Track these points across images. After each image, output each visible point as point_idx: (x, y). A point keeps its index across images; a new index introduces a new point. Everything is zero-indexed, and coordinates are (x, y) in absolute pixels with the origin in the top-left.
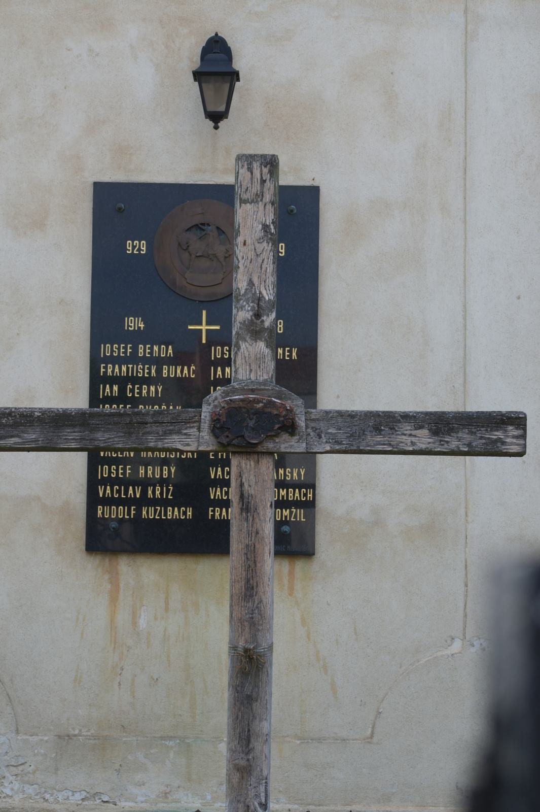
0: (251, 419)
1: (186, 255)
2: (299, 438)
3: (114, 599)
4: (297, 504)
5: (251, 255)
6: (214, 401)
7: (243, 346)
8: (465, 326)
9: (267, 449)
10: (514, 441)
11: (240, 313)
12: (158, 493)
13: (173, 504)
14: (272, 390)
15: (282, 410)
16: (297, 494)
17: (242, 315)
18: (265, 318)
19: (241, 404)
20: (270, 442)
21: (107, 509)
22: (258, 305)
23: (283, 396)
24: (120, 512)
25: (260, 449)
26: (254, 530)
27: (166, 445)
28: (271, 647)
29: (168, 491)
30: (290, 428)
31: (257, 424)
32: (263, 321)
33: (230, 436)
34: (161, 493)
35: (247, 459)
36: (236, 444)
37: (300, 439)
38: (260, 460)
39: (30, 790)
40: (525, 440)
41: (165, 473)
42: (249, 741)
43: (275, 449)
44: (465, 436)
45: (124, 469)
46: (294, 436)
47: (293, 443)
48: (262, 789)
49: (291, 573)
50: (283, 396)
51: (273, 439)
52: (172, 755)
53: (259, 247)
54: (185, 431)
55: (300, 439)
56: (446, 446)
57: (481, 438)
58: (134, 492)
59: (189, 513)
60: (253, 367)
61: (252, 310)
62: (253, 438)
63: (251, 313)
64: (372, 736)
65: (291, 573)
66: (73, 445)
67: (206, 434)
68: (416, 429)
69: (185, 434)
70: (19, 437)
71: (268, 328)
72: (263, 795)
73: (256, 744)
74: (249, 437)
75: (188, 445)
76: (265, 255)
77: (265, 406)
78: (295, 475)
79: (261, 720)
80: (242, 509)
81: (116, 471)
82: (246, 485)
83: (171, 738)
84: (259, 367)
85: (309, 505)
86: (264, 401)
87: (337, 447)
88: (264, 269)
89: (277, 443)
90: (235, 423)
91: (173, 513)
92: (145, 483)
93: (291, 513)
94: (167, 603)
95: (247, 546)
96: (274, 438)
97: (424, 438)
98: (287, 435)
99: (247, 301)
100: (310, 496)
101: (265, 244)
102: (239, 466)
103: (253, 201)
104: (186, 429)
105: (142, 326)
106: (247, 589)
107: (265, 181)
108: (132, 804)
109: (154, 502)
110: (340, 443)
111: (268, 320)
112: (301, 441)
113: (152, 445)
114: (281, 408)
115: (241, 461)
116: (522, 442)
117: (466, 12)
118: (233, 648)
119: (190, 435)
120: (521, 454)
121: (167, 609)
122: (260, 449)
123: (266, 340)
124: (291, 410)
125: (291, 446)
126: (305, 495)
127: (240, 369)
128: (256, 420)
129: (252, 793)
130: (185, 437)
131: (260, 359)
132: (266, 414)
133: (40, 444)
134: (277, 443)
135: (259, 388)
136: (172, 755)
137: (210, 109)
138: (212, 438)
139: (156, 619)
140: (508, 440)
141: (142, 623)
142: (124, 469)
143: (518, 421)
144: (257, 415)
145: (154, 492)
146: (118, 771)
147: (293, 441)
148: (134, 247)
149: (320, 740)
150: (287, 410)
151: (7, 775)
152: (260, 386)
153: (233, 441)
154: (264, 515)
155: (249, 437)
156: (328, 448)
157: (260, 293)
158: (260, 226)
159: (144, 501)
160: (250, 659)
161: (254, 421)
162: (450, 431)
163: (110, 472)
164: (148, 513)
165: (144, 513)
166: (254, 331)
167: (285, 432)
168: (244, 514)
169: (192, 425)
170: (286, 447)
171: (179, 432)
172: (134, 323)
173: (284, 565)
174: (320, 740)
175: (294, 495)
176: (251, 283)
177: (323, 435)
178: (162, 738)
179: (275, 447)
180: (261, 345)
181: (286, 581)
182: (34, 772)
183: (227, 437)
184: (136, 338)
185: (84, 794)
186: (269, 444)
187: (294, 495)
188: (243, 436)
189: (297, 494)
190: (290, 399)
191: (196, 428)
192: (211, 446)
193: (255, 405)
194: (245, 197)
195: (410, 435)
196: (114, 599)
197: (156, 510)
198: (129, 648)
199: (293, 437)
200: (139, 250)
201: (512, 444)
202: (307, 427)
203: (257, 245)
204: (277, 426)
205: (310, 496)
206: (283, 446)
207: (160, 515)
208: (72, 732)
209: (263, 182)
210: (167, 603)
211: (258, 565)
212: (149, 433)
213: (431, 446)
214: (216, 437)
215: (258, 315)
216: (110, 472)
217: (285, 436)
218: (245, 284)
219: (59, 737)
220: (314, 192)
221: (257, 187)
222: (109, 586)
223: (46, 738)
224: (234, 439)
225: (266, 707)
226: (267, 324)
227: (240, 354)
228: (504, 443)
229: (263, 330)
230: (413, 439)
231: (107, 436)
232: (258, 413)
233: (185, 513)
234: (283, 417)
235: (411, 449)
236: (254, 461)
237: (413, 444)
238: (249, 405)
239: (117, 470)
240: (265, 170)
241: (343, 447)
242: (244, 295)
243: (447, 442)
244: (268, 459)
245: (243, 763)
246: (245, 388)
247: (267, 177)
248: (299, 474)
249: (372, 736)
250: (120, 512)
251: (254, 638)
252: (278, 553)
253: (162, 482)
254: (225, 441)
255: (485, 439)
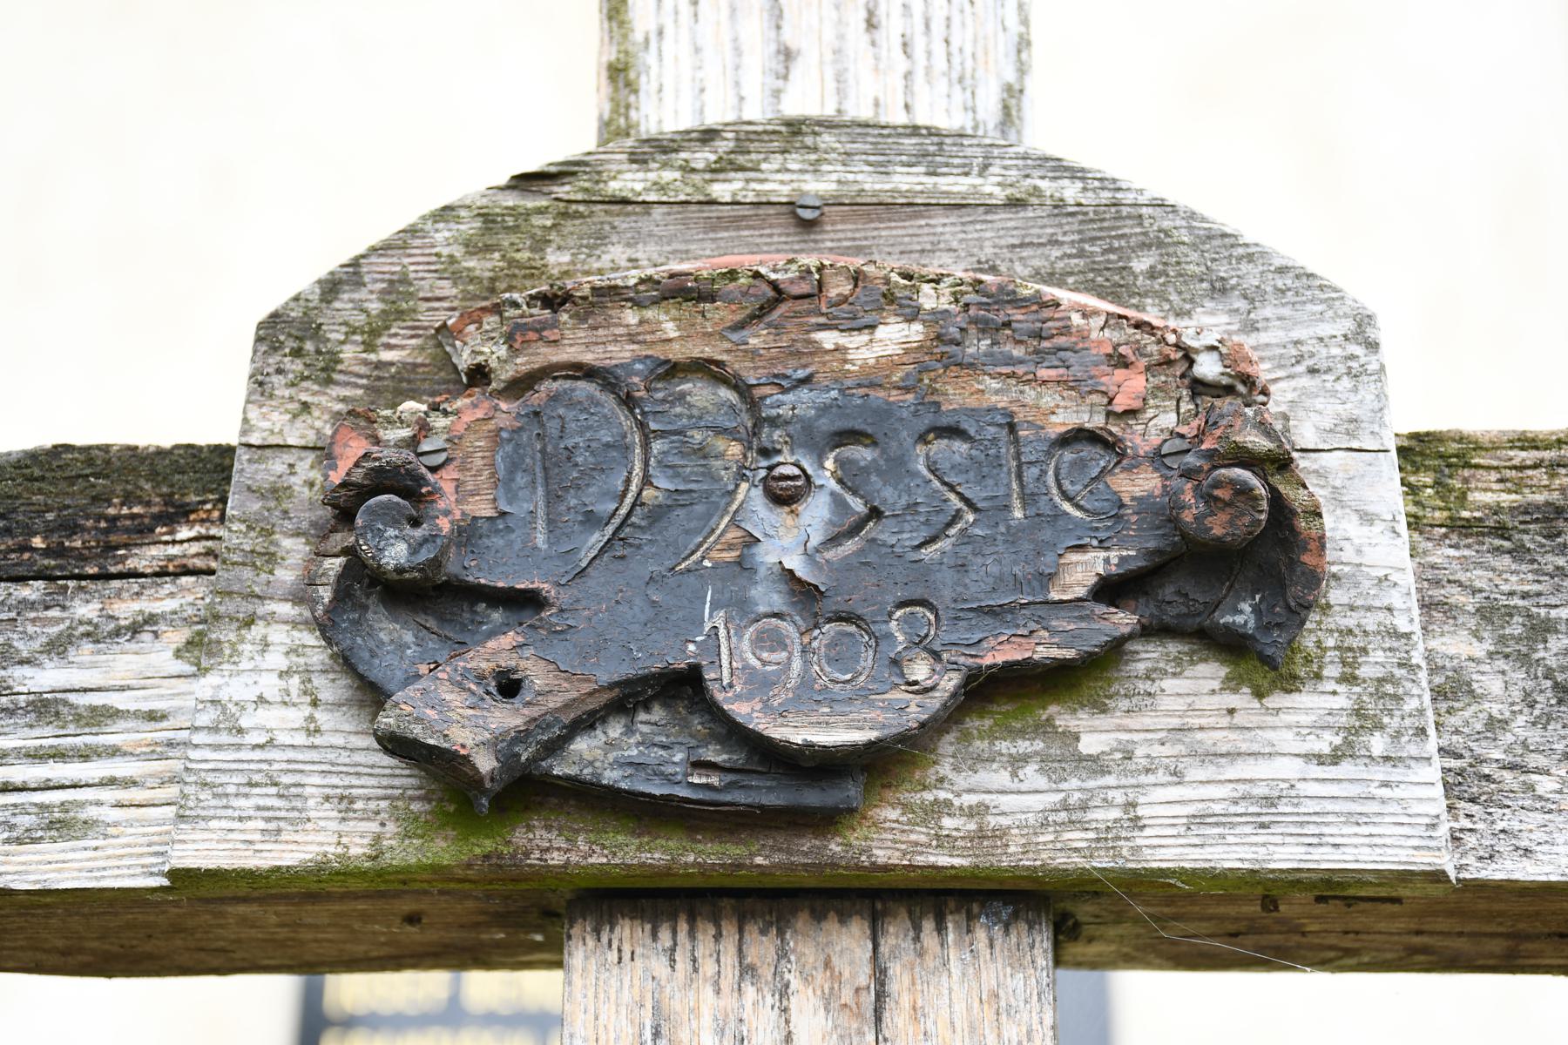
0: (784, 496)
2: (1358, 712)
6: (372, 336)
9: (981, 834)
14: (1015, 204)
15: (1131, 386)
19: (670, 329)
20: (1016, 763)
23: (1141, 264)
31: (850, 546)
33: (537, 676)
35: (747, 971)
36: (611, 776)
37: (1364, 720)
38: (899, 979)
43: (1076, 837)
46: (1290, 683)
47: (1288, 768)
50: (1141, 264)
51: (1045, 729)
54: (47, 677)
55: (1364, 720)
62: (810, 696)
67: (270, 685)
69: (45, 708)
74: (760, 684)
84: (871, 24)
86: (928, 299)
89: (1096, 766)
90: (596, 539)
96: (1065, 718)
98: (1209, 673)
104: (58, 647)
112: (1378, 744)
114: (1123, 363)
115: (677, 1003)
119: (101, 716)
127: (676, 47)
128: (838, 503)
130: (44, 736)
132: (954, 432)
134: (1096, 766)
135: (870, 183)
144: (862, 454)
147: (1286, 740)
150: (1199, 387)
152: (882, 169)
153: (582, 745)
155: (760, 684)
161: (816, 514)
167: (1173, 648)
169: (126, 609)
170: (1199, 819)
179: (1073, 813)
183: (509, 686)
186: (1000, 777)
190: (1220, 289)
191: (179, 637)
192: (325, 816)
193: (828, 339)
199: (1276, 700)
224: (587, 723)
234: (1158, 458)
236: (828, 1000)
238: (757, 339)
244: (989, 978)
246: (721, 190)
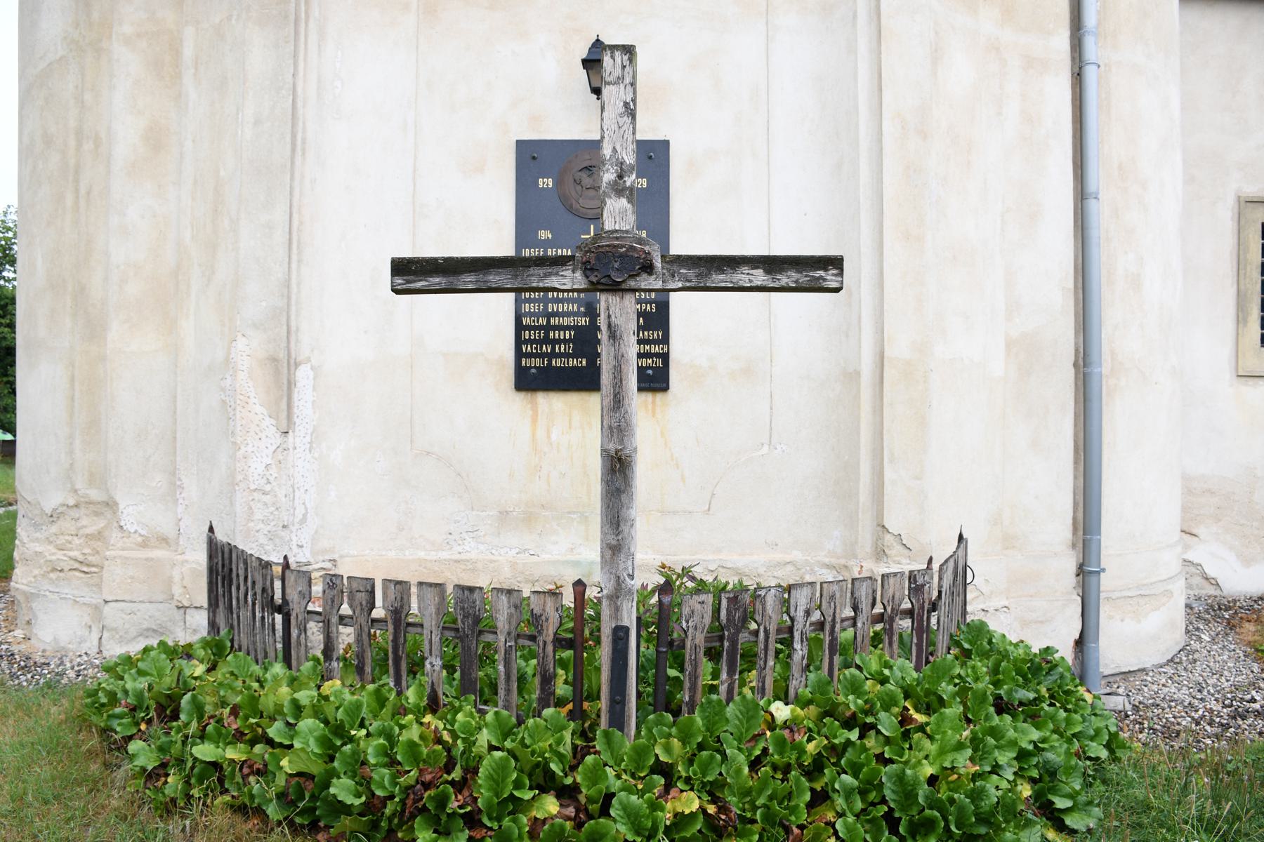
1: (579, 188)
3: (534, 420)
4: (657, 355)
5: (614, 127)
7: (608, 201)
8: (769, 234)
10: (834, 278)
11: (606, 175)
12: (562, 349)
13: (573, 356)
16: (657, 349)
17: (608, 176)
18: (626, 179)
21: (528, 360)
22: (621, 168)
24: (538, 362)
25: (623, 286)
26: (620, 354)
27: (546, 285)
28: (635, 450)
29: (569, 347)
30: (648, 268)
32: (625, 181)
34: (565, 349)
39: (482, 547)
40: (842, 277)
41: (567, 335)
42: (618, 525)
44: (794, 275)
45: (540, 333)
48: (630, 563)
49: (654, 402)
52: (575, 524)
53: (621, 121)
56: (777, 282)
57: (806, 276)
58: (547, 349)
59: (584, 362)
60: (618, 219)
61: (616, 172)
62: (618, 277)
63: (615, 175)
64: (709, 510)
65: (654, 402)
66: (470, 286)
68: (752, 269)
69: (562, 276)
70: (426, 281)
71: (629, 187)
72: (630, 568)
73: (624, 527)
75: (564, 284)
76: (625, 127)
77: (627, 250)
78: (655, 335)
79: (628, 508)
80: (610, 337)
81: (534, 335)
82: (613, 317)
83: (574, 513)
85: (665, 357)
87: (688, 284)
88: (625, 138)
91: (573, 362)
92: (555, 342)
93: (653, 361)
94: (570, 423)
95: (615, 366)
97: (759, 277)
99: (612, 165)
100: (666, 349)
101: (626, 118)
102: (607, 301)
103: (615, 83)
105: (550, 236)
106: (615, 402)
107: (625, 67)
108: (550, 556)
109: (560, 355)
110: (690, 281)
111: (630, 180)
113: (534, 285)
116: (840, 279)
117: (767, 23)
118: (604, 451)
120: (837, 290)
121: (570, 428)
122: (623, 286)
123: (627, 197)
124: (649, 253)
125: (650, 284)
126: (662, 349)
129: (622, 566)
131: (623, 213)
133: (443, 286)
136: (575, 524)
137: (593, 86)
138: (584, 278)
139: (563, 433)
140: (828, 278)
141: (554, 437)
142: (540, 333)
143: (836, 263)
145: (560, 349)
146: (540, 534)
148: (544, 183)
149: (675, 513)
151: (466, 537)
154: (628, 341)
156: (680, 285)
157: (623, 158)
158: (622, 104)
159: (553, 355)
160: (620, 459)
162: (781, 271)
163: (530, 336)
164: (556, 363)
165: (554, 362)
166: (619, 189)
168: (612, 341)
171: (557, 274)
172: (545, 235)
173: (648, 397)
174: (675, 513)
175: (655, 349)
176: (615, 150)
177: (676, 275)
178: (569, 513)
180: (624, 201)
181: (650, 407)
182: (484, 535)
184: (546, 244)
185: (517, 550)
187: (655, 349)
188: (609, 276)
189: (657, 349)
194: (608, 79)
195: (748, 274)
196: (534, 420)
197: (561, 361)
198: (545, 453)
200: (547, 185)
201: (832, 281)
202: (663, 268)
203: (619, 119)
204: (638, 267)
205: (666, 349)
206: (643, 284)
207: (564, 364)
208: (509, 510)
209: (624, 67)
210: (570, 423)
211: (624, 382)
212: (532, 275)
213: (764, 283)
214: (587, 277)
215: (620, 177)
216: (530, 336)
217: (645, 276)
218: (610, 151)
219: (500, 512)
220: (666, 144)
221: (618, 72)
222: (531, 413)
223: (491, 514)
225: (631, 498)
226: (628, 184)
227: (606, 209)
228: (825, 280)
229: (625, 189)
230: (751, 277)
231: (497, 278)
232: (622, 256)
233: (581, 362)
235: (749, 285)
237: (750, 281)
239: (535, 334)
240: (626, 58)
241: (692, 284)
242: (609, 160)
243: (779, 279)
245: (614, 542)
247: (626, 63)
248: (658, 335)
249: (709, 510)
250: (538, 362)
251: (622, 441)
252: (640, 389)
253: (565, 341)
254: (594, 280)
255: (809, 276)
